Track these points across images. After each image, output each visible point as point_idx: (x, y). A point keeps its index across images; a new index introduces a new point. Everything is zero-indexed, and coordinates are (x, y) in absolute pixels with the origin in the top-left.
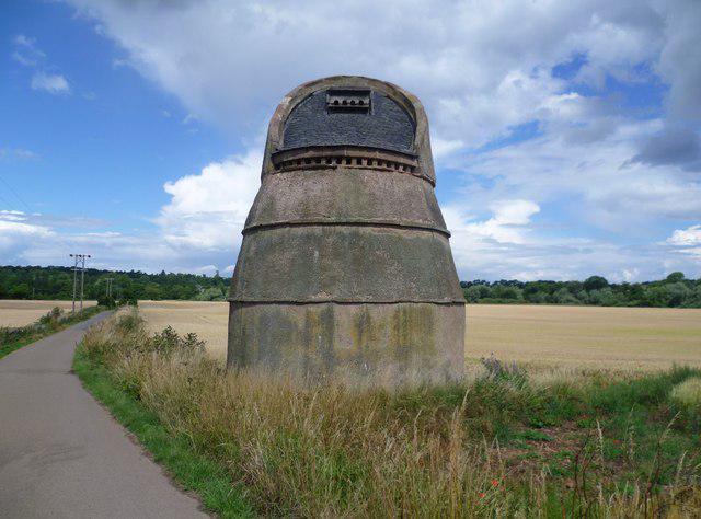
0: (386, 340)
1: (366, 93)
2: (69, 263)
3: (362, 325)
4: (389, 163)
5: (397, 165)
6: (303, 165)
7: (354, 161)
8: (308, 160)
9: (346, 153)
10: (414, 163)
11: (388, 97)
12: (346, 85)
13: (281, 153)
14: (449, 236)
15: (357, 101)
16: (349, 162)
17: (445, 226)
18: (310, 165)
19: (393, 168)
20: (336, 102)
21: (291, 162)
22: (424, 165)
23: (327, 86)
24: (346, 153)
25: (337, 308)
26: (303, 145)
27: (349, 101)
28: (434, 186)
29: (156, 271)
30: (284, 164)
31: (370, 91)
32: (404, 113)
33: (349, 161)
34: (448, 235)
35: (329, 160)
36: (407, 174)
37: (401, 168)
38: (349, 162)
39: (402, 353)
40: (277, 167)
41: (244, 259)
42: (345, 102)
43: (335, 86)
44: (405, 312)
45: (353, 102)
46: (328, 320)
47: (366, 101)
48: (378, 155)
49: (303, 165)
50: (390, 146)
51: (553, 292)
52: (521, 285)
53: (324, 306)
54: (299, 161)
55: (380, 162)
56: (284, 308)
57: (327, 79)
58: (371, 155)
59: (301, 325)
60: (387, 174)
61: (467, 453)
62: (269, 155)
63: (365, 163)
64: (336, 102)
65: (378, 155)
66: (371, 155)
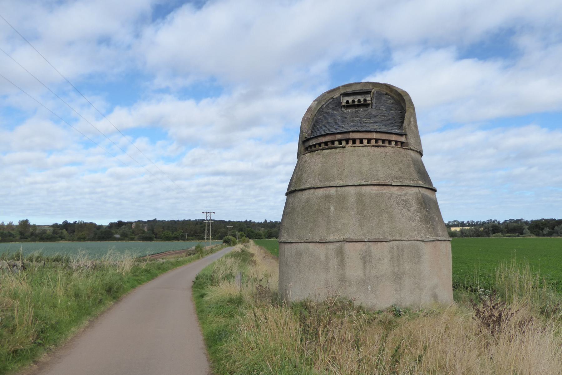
0: (385, 267)
1: (368, 93)
2: (202, 217)
3: (366, 259)
4: (384, 141)
5: (390, 142)
6: (313, 148)
7: (358, 142)
8: (326, 143)
9: (352, 136)
10: (403, 139)
11: (386, 94)
12: (358, 88)
13: (308, 140)
14: (435, 191)
15: (362, 99)
16: (354, 142)
17: (430, 182)
18: (327, 147)
19: (387, 144)
20: (348, 102)
21: (315, 145)
22: (411, 141)
23: (342, 91)
24: (352, 136)
25: (347, 246)
26: (323, 133)
27: (356, 100)
28: (421, 154)
29: (262, 220)
30: (310, 146)
31: (370, 92)
32: (398, 104)
33: (354, 142)
34: (435, 191)
35: (340, 142)
36: (398, 148)
37: (393, 144)
38: (354, 142)
39: (397, 278)
40: (307, 149)
41: (286, 213)
42: (353, 101)
43: (349, 90)
44: (398, 248)
45: (359, 101)
46: (340, 253)
47: (369, 99)
48: (375, 136)
49: (313, 148)
50: (384, 129)
51: (554, 227)
52: (526, 223)
53: (338, 244)
54: (320, 144)
55: (377, 140)
56: (311, 246)
57: (342, 86)
58: (369, 136)
59: (323, 258)
60: (382, 149)
61: (537, 324)
62: (301, 142)
63: (336, 143)
64: (348, 102)
65: (375, 136)
66: (369, 136)
